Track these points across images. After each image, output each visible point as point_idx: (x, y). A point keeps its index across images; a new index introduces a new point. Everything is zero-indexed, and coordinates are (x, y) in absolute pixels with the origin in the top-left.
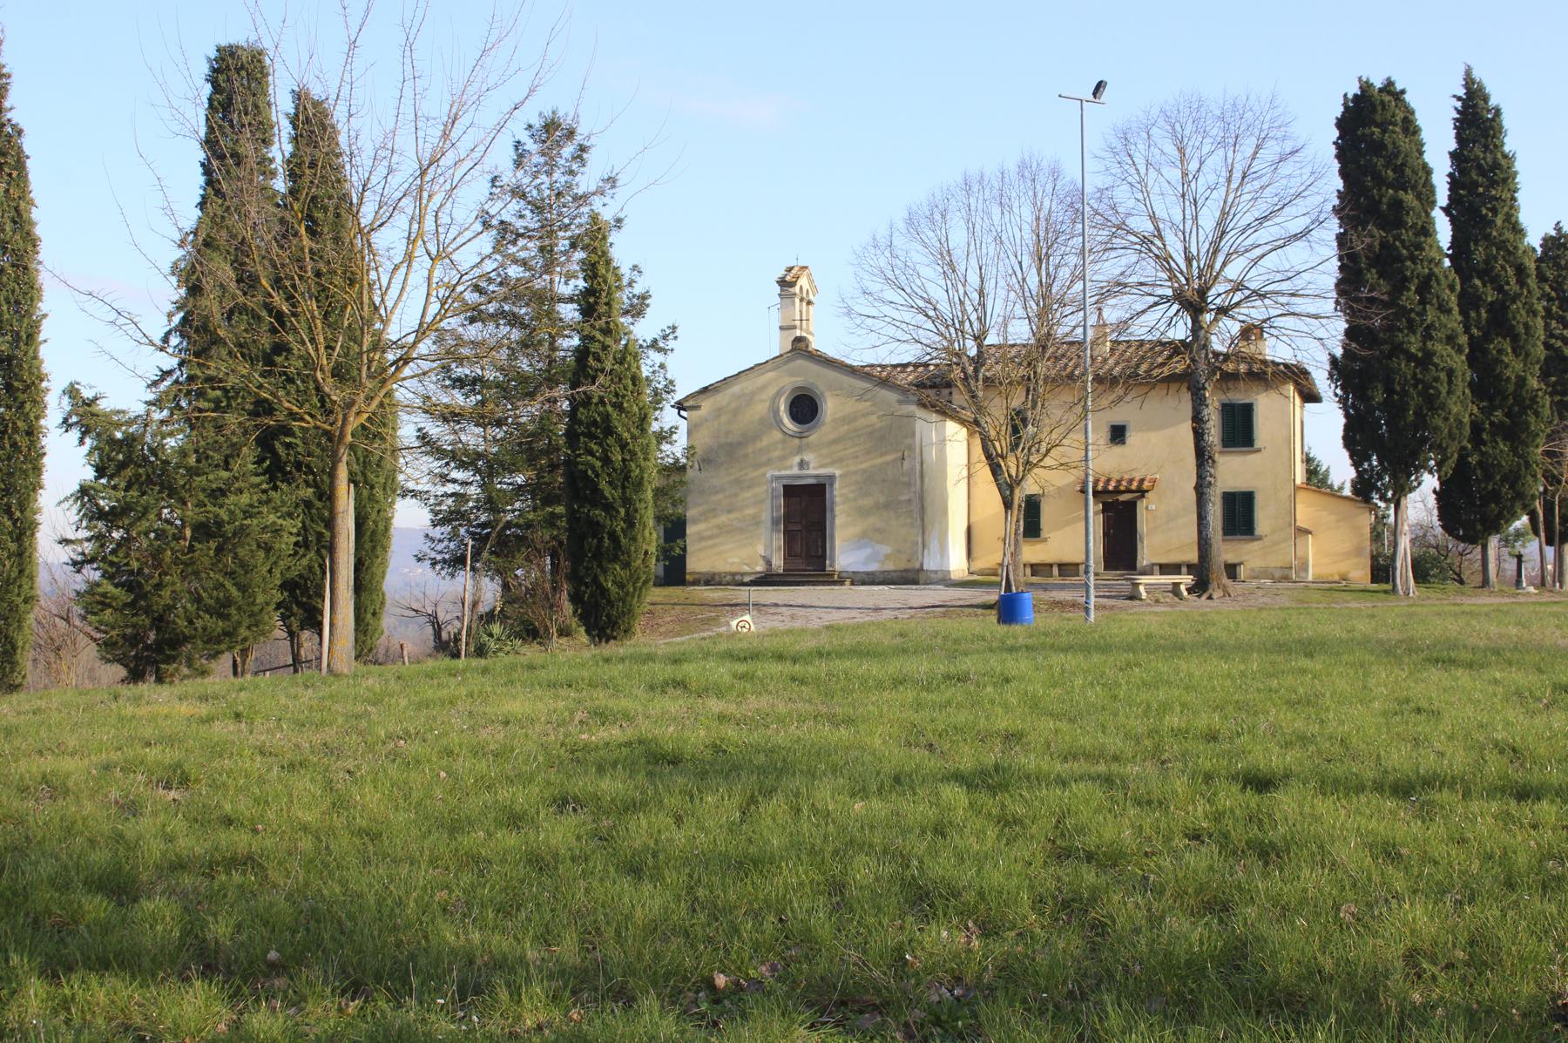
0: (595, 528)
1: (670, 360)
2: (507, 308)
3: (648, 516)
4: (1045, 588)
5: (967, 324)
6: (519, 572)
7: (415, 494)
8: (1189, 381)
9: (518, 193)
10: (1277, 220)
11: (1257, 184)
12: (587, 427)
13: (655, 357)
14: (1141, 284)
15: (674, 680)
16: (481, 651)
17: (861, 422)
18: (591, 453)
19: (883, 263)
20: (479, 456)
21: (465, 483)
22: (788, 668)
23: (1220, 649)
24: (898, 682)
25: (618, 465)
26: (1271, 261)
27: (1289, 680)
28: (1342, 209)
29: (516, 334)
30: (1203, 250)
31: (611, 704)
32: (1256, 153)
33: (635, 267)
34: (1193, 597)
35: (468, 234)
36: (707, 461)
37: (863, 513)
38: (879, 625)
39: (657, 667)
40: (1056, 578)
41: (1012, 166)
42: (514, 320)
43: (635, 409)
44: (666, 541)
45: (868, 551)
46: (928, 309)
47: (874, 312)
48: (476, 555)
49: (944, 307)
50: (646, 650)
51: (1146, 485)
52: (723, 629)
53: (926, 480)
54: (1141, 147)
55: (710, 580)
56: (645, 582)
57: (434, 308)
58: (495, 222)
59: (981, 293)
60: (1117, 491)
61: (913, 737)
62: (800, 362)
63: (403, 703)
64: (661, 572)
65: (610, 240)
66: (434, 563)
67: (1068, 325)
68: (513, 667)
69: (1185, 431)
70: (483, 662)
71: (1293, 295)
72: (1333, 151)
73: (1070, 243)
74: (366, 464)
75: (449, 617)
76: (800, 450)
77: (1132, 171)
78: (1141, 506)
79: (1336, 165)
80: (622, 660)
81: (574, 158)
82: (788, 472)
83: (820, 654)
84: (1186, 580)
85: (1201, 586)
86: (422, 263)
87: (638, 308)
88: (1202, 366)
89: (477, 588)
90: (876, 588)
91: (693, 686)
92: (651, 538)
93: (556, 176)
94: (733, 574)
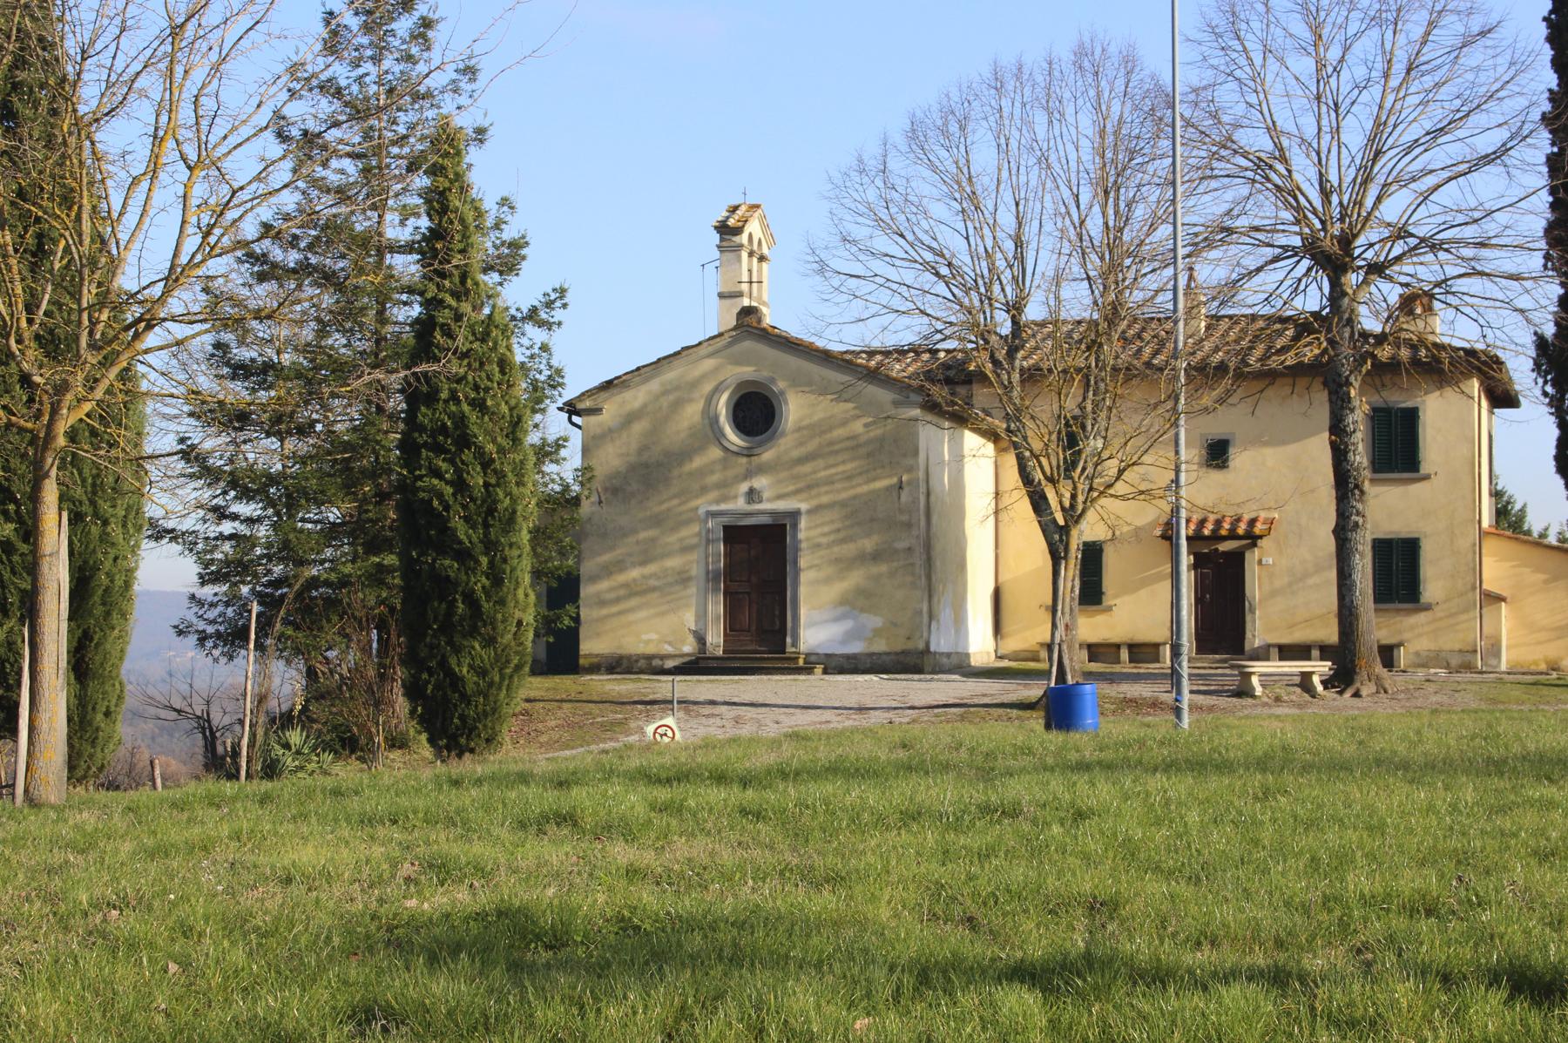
0: (444, 586)
1: (557, 339)
2: (313, 261)
3: (523, 567)
4: (1111, 678)
5: (996, 288)
6: (331, 654)
7: (174, 535)
8: (1326, 376)
9: (331, 89)
10: (1460, 133)
11: (1428, 81)
12: (433, 435)
13: (535, 334)
14: (1257, 229)
15: (557, 815)
16: (271, 770)
17: (839, 433)
18: (437, 474)
19: (872, 195)
20: (272, 480)
21: (250, 521)
22: (734, 795)
23: (1386, 765)
24: (911, 816)
25: (479, 492)
26: (1449, 195)
27: (1530, 819)
28: (1557, 117)
29: (328, 300)
30: (1349, 179)
31: (456, 849)
32: (1427, 33)
33: (504, 202)
34: (1331, 694)
35: (246, 131)
36: (618, 490)
37: (845, 565)
38: (868, 732)
39: (531, 792)
40: (1125, 666)
41: (1064, 53)
42: (328, 279)
43: (504, 408)
44: (550, 606)
45: (848, 624)
46: (942, 267)
47: (858, 269)
48: (265, 624)
49: (963, 258)
50: (513, 768)
51: (1259, 528)
52: (633, 739)
53: (935, 519)
54: (1256, 25)
55: (618, 665)
56: (518, 667)
57: (192, 243)
58: (295, 132)
59: (1019, 243)
60: (1216, 537)
61: (939, 905)
62: (748, 344)
63: (127, 847)
64: (542, 655)
65: (467, 160)
66: (203, 638)
67: (1149, 290)
68: (310, 793)
69: (1318, 449)
70: (267, 785)
71: (1483, 245)
72: (1542, 30)
73: (1150, 168)
74: (96, 488)
75: (227, 720)
76: (748, 474)
77: (1242, 61)
78: (1252, 558)
79: (1547, 53)
80: (479, 782)
81: (414, 37)
83: (784, 775)
84: (1320, 668)
85: (1342, 679)
86: (174, 175)
87: (509, 260)
88: (1346, 350)
89: (263, 674)
90: (860, 678)
91: (588, 822)
92: (525, 605)
93: (387, 63)
94: (650, 658)
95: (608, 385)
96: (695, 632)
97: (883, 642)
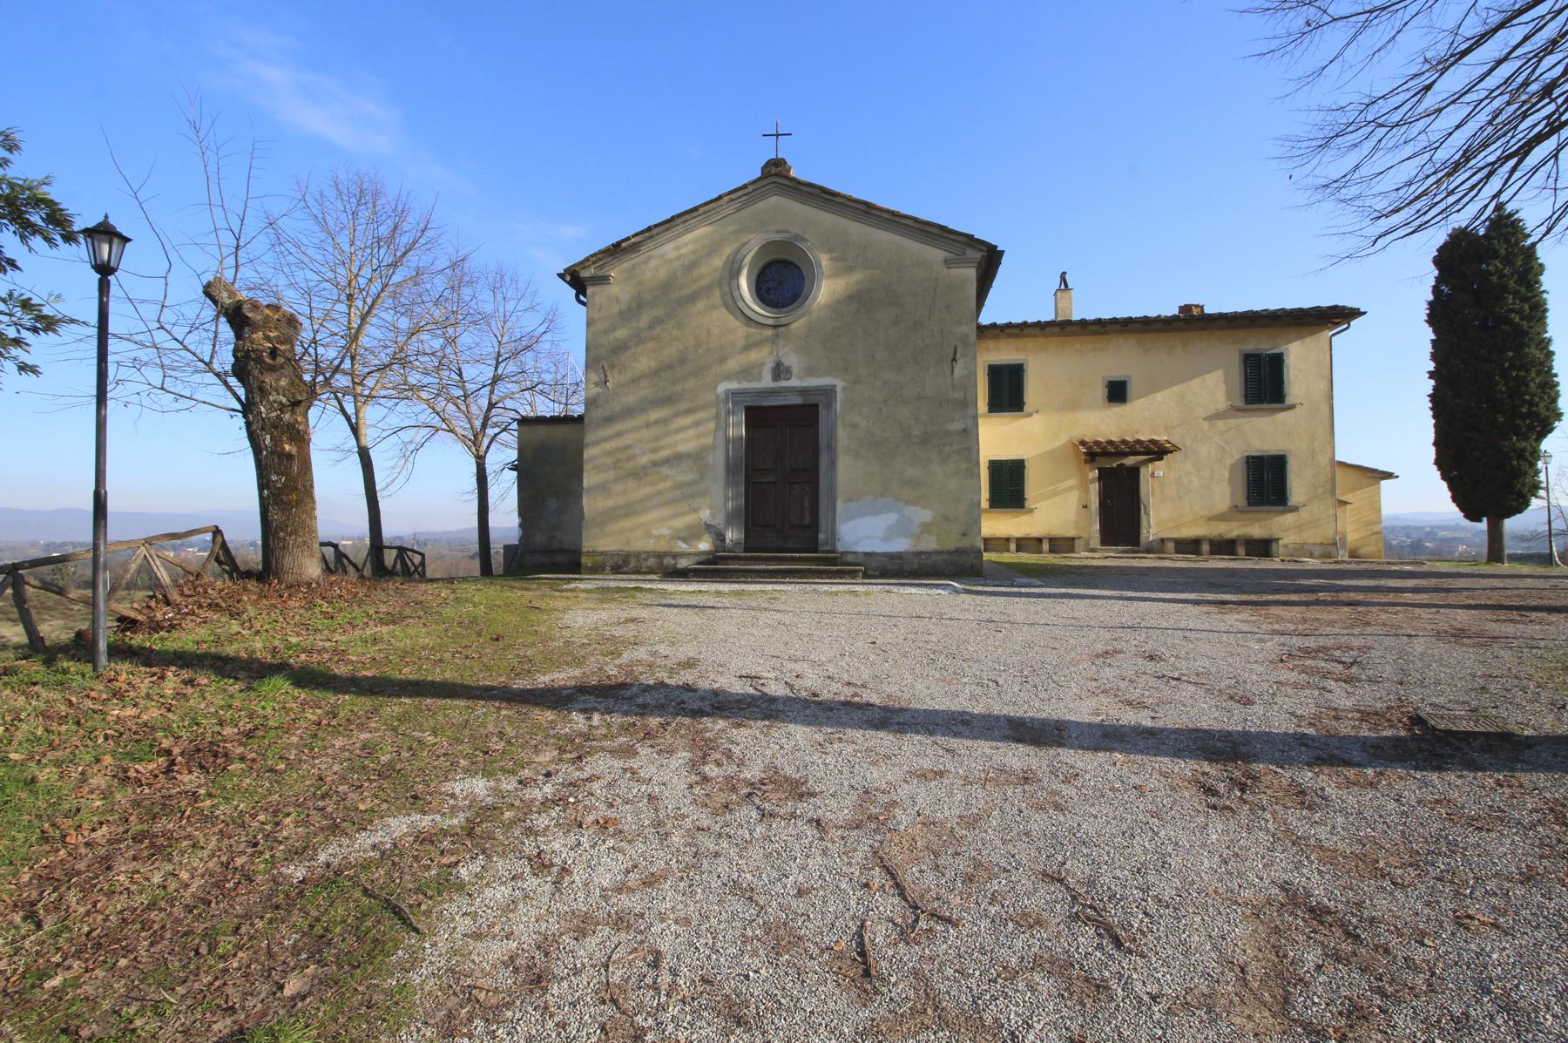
45: (891, 518)
55: (621, 564)
62: (775, 201)
82: (755, 385)
94: (660, 556)
97: (934, 538)
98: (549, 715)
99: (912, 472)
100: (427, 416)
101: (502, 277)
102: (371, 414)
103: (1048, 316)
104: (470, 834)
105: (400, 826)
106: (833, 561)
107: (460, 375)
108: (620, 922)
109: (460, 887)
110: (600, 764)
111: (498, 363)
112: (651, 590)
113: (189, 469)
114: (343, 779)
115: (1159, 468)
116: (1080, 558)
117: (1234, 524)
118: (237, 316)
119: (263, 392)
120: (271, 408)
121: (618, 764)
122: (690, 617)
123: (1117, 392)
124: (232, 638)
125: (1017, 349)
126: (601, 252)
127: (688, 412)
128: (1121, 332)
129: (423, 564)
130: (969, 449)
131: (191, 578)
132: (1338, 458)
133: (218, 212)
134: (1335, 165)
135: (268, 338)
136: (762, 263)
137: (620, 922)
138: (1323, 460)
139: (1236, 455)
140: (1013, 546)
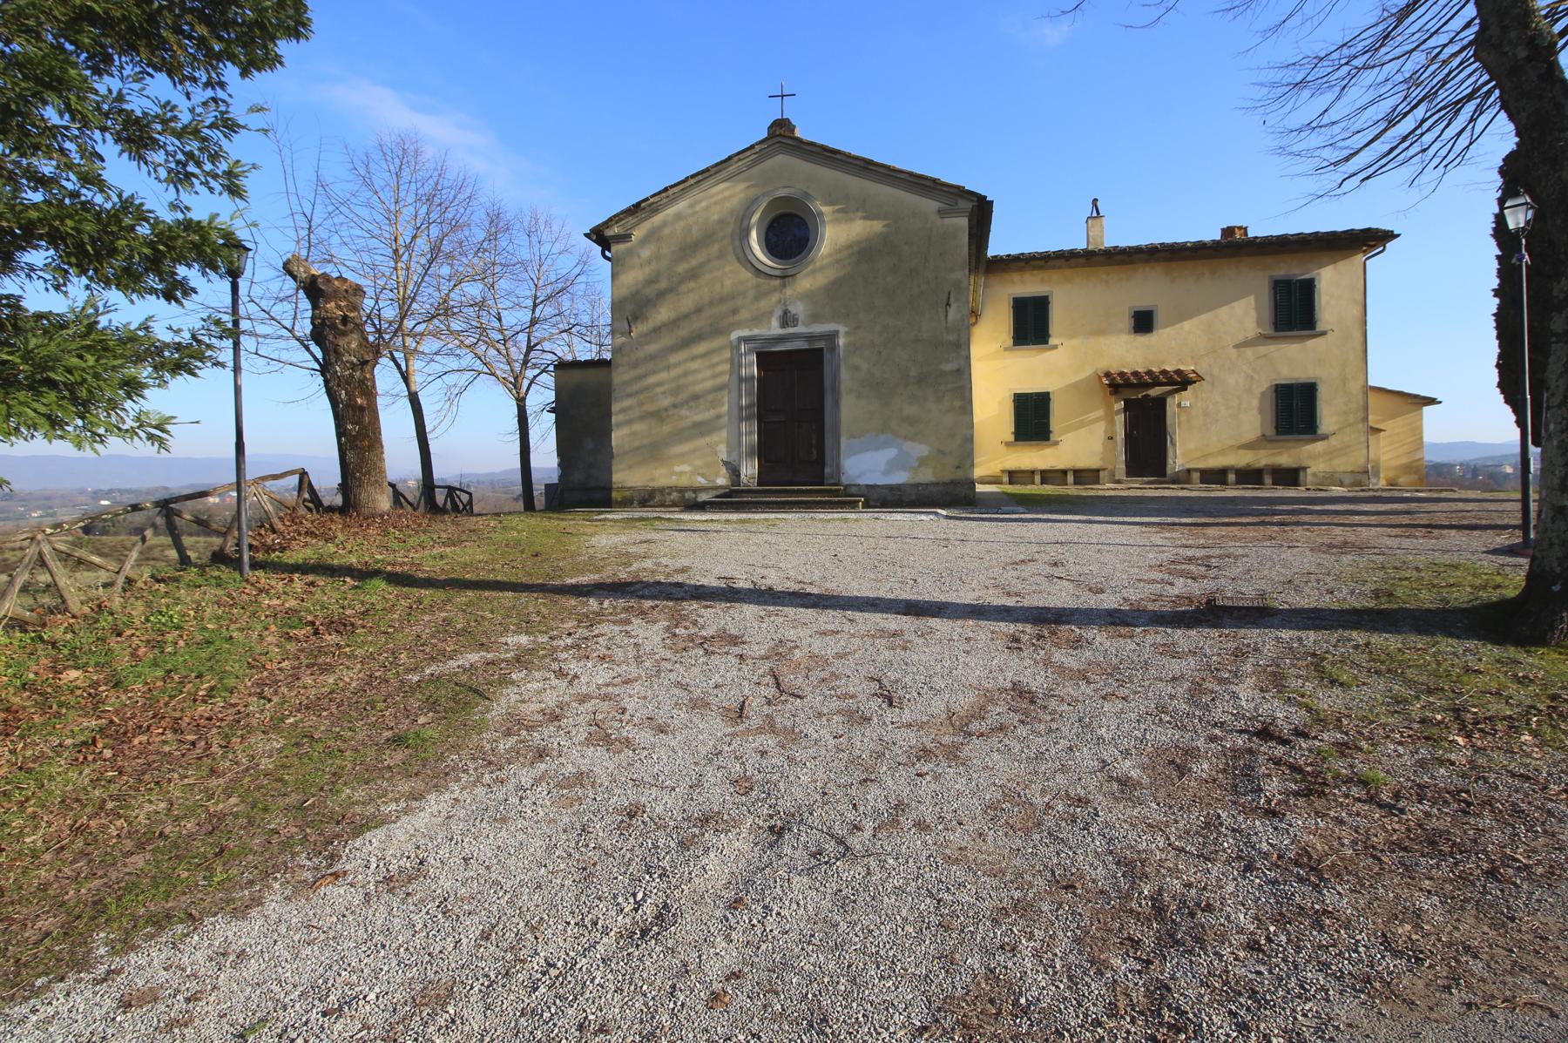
45: (892, 452)
55: (647, 498)
62: (780, 159)
94: (682, 490)
95: (636, 208)
96: (726, 463)
97: (930, 471)
98: (573, 602)
99: (910, 410)
100: (468, 360)
101: (537, 220)
102: (416, 364)
103: (1080, 244)
104: (518, 661)
105: (474, 657)
106: (836, 493)
107: (500, 320)
108: (606, 698)
109: (513, 683)
110: (605, 628)
111: (535, 306)
112: (669, 520)
113: (291, 424)
114: (433, 637)
115: (1186, 398)
116: (1106, 489)
117: (1263, 453)
118: (314, 289)
119: (338, 355)
120: (345, 368)
121: (617, 628)
122: (696, 539)
123: (1143, 322)
124: (332, 556)
125: (1042, 281)
126: (623, 212)
127: (704, 356)
128: (1147, 261)
129: (470, 502)
130: (962, 387)
131: (292, 514)
132: (1371, 383)
133: (293, 199)
134: (1308, 107)
135: (339, 307)
136: (768, 219)
137: (606, 698)
138: (1355, 387)
139: (1264, 383)
140: (1038, 478)
